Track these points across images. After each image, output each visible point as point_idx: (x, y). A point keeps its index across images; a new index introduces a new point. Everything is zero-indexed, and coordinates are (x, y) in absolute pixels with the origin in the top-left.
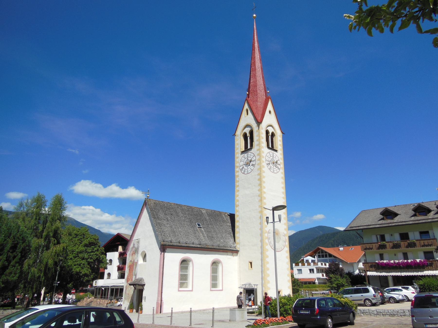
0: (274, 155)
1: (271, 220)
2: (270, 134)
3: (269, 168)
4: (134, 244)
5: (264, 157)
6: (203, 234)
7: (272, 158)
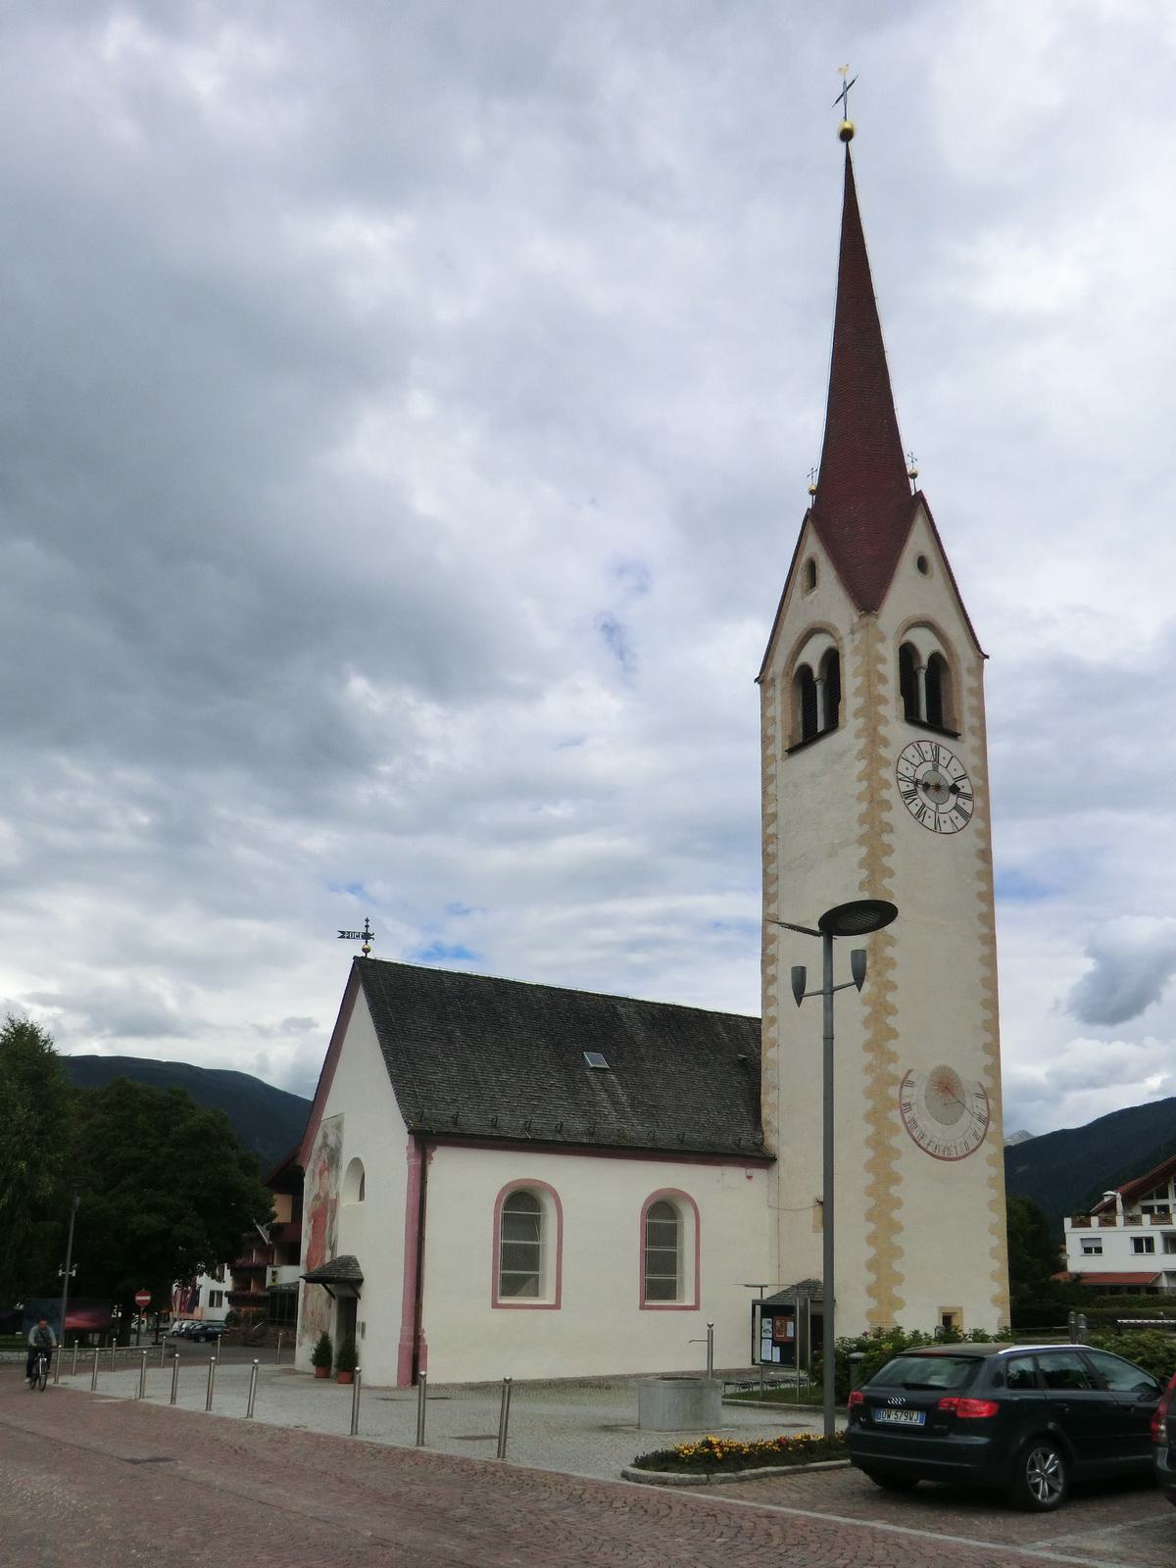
0: (943, 753)
1: (814, 982)
2: (925, 661)
3: (914, 809)
4: (325, 1136)
5: (887, 764)
6: (612, 1095)
7: (928, 766)
